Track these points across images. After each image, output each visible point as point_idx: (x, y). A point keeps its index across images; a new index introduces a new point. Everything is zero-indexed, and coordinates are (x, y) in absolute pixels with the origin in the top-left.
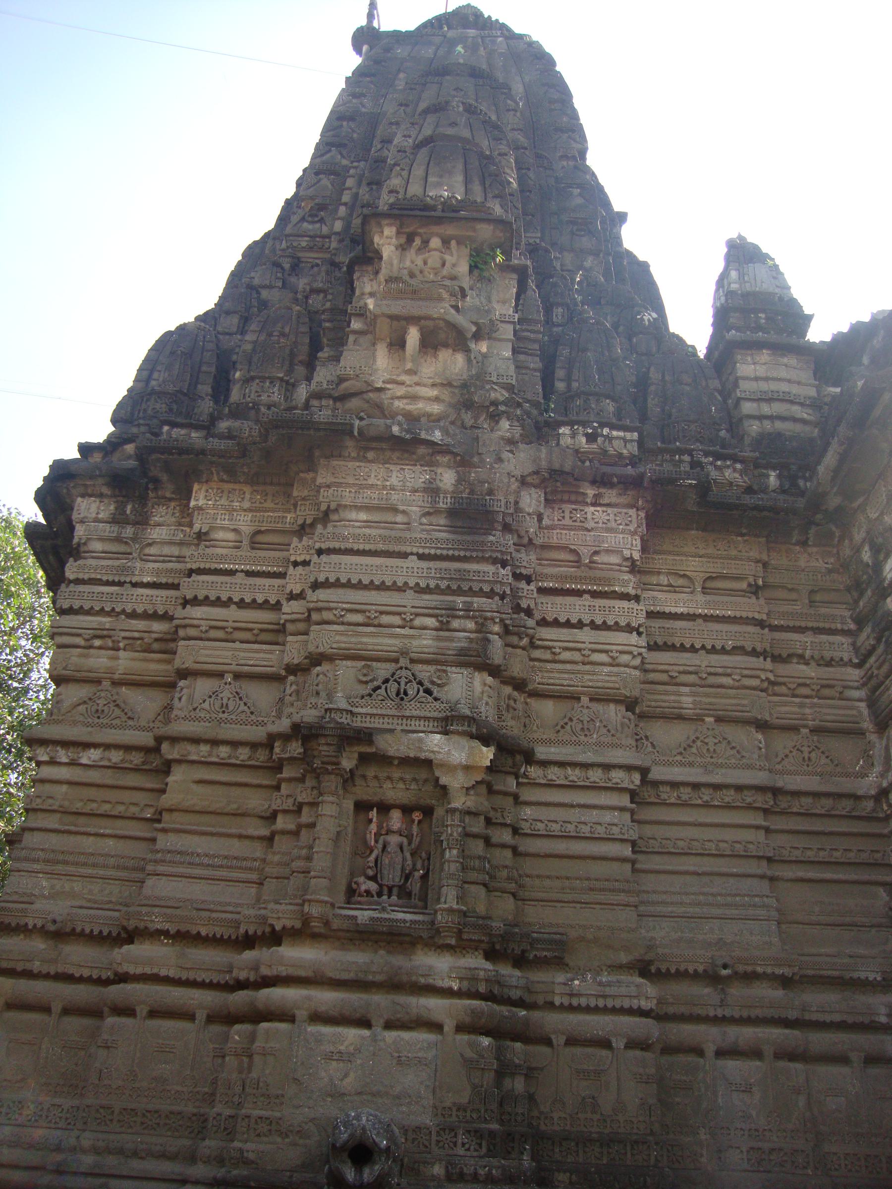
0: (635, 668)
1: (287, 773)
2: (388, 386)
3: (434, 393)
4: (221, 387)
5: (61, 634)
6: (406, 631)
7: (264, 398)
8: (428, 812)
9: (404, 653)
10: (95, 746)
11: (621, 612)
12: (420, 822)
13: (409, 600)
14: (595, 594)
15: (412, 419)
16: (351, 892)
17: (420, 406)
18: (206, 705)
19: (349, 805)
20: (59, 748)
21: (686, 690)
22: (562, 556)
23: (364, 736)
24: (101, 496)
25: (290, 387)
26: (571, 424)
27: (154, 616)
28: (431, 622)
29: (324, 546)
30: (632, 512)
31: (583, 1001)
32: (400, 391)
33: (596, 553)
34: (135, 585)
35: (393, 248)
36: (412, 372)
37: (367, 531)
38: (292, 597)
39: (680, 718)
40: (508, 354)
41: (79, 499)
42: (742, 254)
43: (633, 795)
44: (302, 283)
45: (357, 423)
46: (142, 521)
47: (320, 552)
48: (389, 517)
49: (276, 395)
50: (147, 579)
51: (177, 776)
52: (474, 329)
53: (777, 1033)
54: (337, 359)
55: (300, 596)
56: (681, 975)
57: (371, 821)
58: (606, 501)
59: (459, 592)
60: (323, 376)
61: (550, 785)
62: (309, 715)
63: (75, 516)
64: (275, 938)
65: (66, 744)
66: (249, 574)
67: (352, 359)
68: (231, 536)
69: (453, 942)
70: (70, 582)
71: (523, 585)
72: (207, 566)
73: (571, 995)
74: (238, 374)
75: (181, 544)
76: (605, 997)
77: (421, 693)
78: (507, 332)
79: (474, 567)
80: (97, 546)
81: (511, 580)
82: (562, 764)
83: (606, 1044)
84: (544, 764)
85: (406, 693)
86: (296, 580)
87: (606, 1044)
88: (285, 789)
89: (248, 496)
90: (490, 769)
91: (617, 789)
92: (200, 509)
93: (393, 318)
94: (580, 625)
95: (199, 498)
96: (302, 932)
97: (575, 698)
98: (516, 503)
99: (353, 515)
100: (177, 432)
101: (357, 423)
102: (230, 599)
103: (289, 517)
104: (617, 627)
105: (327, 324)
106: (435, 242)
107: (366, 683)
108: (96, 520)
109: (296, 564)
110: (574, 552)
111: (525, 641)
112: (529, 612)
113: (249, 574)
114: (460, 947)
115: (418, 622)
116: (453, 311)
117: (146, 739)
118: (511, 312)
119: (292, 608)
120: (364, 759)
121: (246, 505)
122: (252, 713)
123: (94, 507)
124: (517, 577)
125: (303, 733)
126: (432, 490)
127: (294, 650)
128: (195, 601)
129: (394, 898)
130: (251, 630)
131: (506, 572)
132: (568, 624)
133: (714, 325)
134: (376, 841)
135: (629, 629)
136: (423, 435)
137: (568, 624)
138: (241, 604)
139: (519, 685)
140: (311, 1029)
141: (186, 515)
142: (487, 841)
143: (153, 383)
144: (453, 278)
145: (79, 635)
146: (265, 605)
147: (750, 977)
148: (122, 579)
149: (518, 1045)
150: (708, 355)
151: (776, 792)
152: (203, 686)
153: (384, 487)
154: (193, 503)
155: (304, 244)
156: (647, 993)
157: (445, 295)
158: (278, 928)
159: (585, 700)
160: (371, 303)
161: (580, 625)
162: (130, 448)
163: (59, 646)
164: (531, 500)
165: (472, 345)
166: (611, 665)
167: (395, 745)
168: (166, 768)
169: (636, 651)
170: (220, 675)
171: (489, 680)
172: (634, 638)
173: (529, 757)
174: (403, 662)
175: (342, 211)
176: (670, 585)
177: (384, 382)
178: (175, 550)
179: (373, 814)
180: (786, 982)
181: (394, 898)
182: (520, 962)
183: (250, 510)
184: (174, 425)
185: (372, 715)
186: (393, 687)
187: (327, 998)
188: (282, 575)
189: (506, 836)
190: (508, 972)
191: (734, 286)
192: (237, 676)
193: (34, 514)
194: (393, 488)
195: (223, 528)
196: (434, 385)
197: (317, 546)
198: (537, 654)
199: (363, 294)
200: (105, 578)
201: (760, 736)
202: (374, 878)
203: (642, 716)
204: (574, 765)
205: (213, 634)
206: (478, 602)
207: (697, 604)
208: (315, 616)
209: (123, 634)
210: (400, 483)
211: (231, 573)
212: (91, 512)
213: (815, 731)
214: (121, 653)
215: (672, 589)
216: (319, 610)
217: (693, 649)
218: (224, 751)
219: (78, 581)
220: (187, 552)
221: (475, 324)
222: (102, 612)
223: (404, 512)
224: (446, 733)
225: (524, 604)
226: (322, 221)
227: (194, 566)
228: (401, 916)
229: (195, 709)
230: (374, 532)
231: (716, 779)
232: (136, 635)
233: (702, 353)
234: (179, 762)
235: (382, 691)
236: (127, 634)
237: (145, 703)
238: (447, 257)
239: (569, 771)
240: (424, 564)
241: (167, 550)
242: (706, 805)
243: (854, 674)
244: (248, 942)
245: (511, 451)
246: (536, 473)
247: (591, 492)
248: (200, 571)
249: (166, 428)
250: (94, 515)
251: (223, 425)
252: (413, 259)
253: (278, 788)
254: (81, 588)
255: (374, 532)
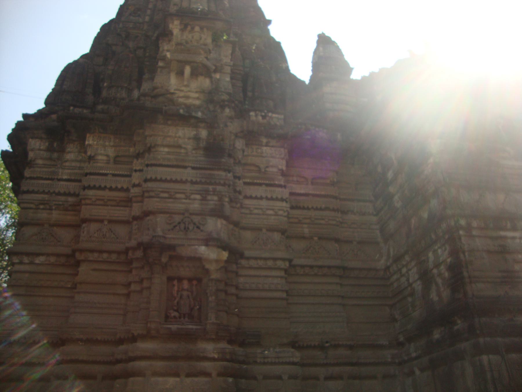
0: (285, 216)
1: (135, 265)
2: (177, 92)
3: (197, 95)
4: (97, 90)
5: (23, 203)
6: (187, 201)
7: (118, 95)
8: (199, 280)
9: (187, 210)
10: (42, 254)
11: (278, 192)
12: (196, 285)
13: (188, 187)
14: (267, 185)
15: (188, 107)
16: (167, 317)
17: (190, 101)
18: (96, 235)
19: (165, 278)
20: (24, 256)
21: (306, 226)
22: (253, 168)
23: (172, 248)
24: (41, 139)
25: (130, 91)
26: (255, 111)
27: (69, 194)
28: (198, 197)
29: (149, 163)
30: (282, 150)
31: (269, 360)
32: (182, 94)
33: (267, 167)
34: (59, 180)
35: (178, 30)
36: (187, 86)
37: (169, 156)
38: (134, 186)
39: (304, 238)
40: (228, 79)
41: (30, 140)
42: (323, 41)
43: (286, 271)
44: (131, 44)
45: (164, 108)
46: (62, 150)
47: (147, 165)
48: (178, 150)
49: (124, 94)
50: (65, 177)
51: (83, 268)
52: (214, 68)
53: (348, 369)
54: (152, 79)
55: (139, 185)
56: (309, 347)
57: (174, 285)
58: (271, 144)
59: (210, 184)
60: (146, 86)
61: (251, 268)
62: (146, 238)
63: (29, 148)
64: (134, 339)
65: (28, 254)
66: (114, 175)
67: (159, 79)
68: (105, 158)
69: (214, 337)
70: (27, 178)
71: (237, 181)
72: (94, 171)
73: (265, 358)
74: (105, 84)
75: (80, 161)
76: (278, 358)
77: (195, 228)
78: (228, 69)
79: (216, 172)
80: (40, 162)
81: (232, 178)
82: (256, 259)
83: (280, 378)
84: (248, 259)
85: (188, 228)
86: (136, 178)
87: (280, 378)
88: (134, 272)
89: (112, 140)
90: (227, 261)
91: (279, 269)
92: (90, 145)
93: (179, 61)
94: (261, 198)
95: (90, 140)
96: (147, 336)
97: (260, 229)
98: (234, 145)
99: (162, 149)
100: (77, 110)
101: (164, 108)
102: (187, 180)
103: (132, 150)
104: (277, 199)
105: (147, 63)
106: (197, 29)
107: (170, 224)
108: (40, 150)
109: (136, 171)
110: (257, 166)
111: (239, 205)
112: (240, 193)
113: (114, 175)
114: (217, 339)
115: (193, 197)
116: (205, 60)
117: (68, 251)
118: (229, 61)
119: (134, 191)
120: (171, 258)
121: (112, 144)
122: (117, 238)
123: (38, 144)
124: (235, 177)
125: (145, 247)
126: (197, 138)
127: (136, 209)
128: (89, 188)
129: (187, 319)
130: (115, 201)
131: (230, 175)
132: (256, 198)
133: (313, 71)
134: (177, 294)
135: (282, 200)
136: (194, 114)
137: (256, 198)
138: (111, 189)
139: (236, 224)
140: (153, 379)
141: (83, 148)
142: (226, 292)
143: (64, 87)
144: (205, 45)
145: (32, 203)
146: (122, 190)
147: (336, 346)
148: (53, 177)
149: (243, 381)
150: (12, 147)
151: (344, 268)
152: (94, 226)
153: (176, 137)
154: (87, 143)
155: (131, 26)
156: (297, 356)
157: (202, 52)
158: (136, 334)
159: (264, 230)
160: (168, 55)
161: (261, 198)
162: (54, 116)
163: (22, 208)
164: (239, 144)
165: (213, 75)
166: (275, 215)
167: (185, 252)
168: (78, 264)
169: (285, 209)
170: (102, 221)
171: (224, 222)
172: (284, 204)
173: (242, 256)
174: (186, 215)
175: (149, 12)
176: (298, 181)
177: (175, 90)
178: (78, 164)
179: (175, 282)
180: (351, 347)
181: (187, 319)
182: (242, 344)
183: (113, 146)
184: (75, 106)
185: (174, 238)
186: (182, 226)
187: (159, 365)
188: (130, 176)
189: (233, 290)
190: (240, 351)
191: (322, 54)
192: (110, 221)
193: (7, 146)
194: (179, 137)
195: (101, 154)
196: (196, 92)
197: (146, 162)
198: (243, 211)
199: (163, 50)
200: (44, 177)
201: (337, 245)
202: (177, 311)
203: (288, 237)
204: (261, 259)
205: (98, 202)
206: (219, 188)
207: (309, 189)
208: (146, 194)
209: (54, 203)
210: (183, 134)
211: (106, 175)
212: (36, 145)
213: (359, 243)
214: (54, 212)
215: (298, 182)
216: (148, 192)
217: (308, 209)
218: (105, 255)
219: (31, 178)
220: (83, 165)
221: (215, 66)
222: (44, 192)
223: (185, 148)
224: (207, 245)
225: (238, 189)
226: (139, 16)
227: (88, 171)
228: (190, 327)
229: (90, 237)
230: (172, 157)
231: (320, 263)
232: (61, 203)
233: (11, 150)
234: (84, 261)
235: (178, 228)
236: (57, 203)
237: (66, 235)
238: (202, 35)
239: (259, 261)
240: (194, 171)
241: (74, 164)
242: (316, 275)
243: (374, 219)
244: (121, 342)
245: (231, 122)
246: (242, 132)
247: (264, 140)
248: (91, 174)
249: (72, 108)
250: (38, 147)
251: (100, 107)
252: (187, 36)
253: (131, 271)
254: (33, 181)
255: (172, 157)
